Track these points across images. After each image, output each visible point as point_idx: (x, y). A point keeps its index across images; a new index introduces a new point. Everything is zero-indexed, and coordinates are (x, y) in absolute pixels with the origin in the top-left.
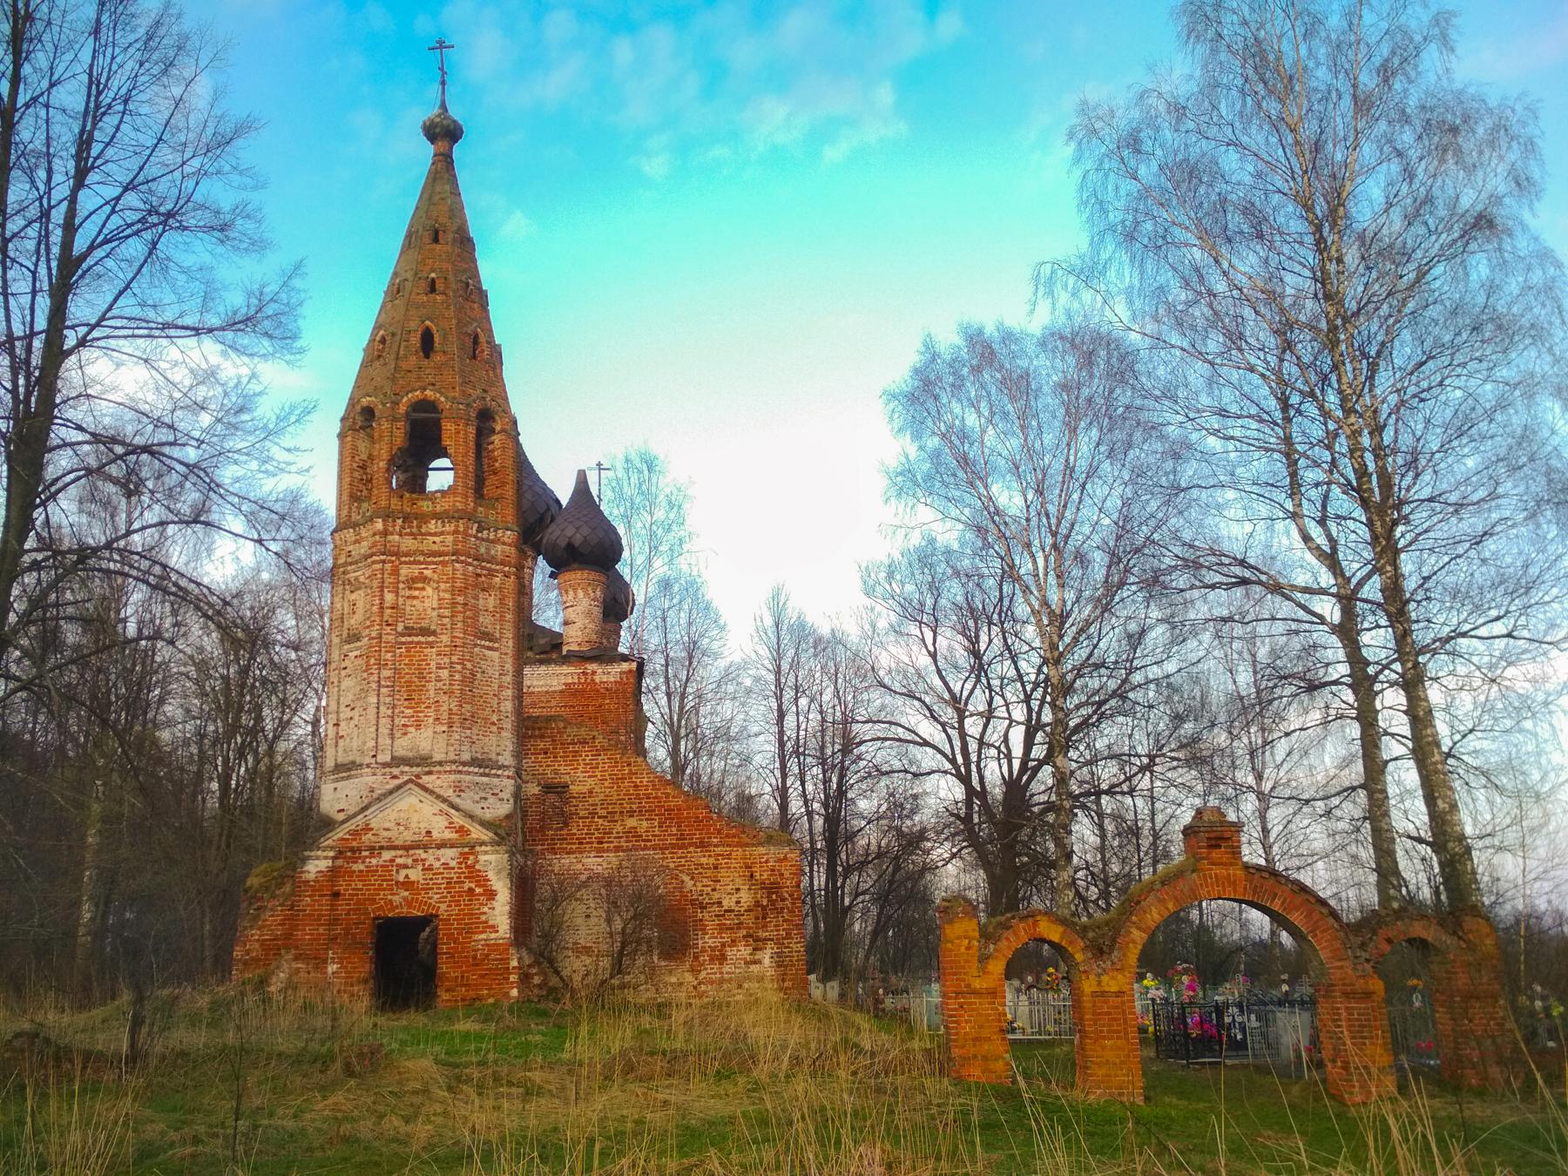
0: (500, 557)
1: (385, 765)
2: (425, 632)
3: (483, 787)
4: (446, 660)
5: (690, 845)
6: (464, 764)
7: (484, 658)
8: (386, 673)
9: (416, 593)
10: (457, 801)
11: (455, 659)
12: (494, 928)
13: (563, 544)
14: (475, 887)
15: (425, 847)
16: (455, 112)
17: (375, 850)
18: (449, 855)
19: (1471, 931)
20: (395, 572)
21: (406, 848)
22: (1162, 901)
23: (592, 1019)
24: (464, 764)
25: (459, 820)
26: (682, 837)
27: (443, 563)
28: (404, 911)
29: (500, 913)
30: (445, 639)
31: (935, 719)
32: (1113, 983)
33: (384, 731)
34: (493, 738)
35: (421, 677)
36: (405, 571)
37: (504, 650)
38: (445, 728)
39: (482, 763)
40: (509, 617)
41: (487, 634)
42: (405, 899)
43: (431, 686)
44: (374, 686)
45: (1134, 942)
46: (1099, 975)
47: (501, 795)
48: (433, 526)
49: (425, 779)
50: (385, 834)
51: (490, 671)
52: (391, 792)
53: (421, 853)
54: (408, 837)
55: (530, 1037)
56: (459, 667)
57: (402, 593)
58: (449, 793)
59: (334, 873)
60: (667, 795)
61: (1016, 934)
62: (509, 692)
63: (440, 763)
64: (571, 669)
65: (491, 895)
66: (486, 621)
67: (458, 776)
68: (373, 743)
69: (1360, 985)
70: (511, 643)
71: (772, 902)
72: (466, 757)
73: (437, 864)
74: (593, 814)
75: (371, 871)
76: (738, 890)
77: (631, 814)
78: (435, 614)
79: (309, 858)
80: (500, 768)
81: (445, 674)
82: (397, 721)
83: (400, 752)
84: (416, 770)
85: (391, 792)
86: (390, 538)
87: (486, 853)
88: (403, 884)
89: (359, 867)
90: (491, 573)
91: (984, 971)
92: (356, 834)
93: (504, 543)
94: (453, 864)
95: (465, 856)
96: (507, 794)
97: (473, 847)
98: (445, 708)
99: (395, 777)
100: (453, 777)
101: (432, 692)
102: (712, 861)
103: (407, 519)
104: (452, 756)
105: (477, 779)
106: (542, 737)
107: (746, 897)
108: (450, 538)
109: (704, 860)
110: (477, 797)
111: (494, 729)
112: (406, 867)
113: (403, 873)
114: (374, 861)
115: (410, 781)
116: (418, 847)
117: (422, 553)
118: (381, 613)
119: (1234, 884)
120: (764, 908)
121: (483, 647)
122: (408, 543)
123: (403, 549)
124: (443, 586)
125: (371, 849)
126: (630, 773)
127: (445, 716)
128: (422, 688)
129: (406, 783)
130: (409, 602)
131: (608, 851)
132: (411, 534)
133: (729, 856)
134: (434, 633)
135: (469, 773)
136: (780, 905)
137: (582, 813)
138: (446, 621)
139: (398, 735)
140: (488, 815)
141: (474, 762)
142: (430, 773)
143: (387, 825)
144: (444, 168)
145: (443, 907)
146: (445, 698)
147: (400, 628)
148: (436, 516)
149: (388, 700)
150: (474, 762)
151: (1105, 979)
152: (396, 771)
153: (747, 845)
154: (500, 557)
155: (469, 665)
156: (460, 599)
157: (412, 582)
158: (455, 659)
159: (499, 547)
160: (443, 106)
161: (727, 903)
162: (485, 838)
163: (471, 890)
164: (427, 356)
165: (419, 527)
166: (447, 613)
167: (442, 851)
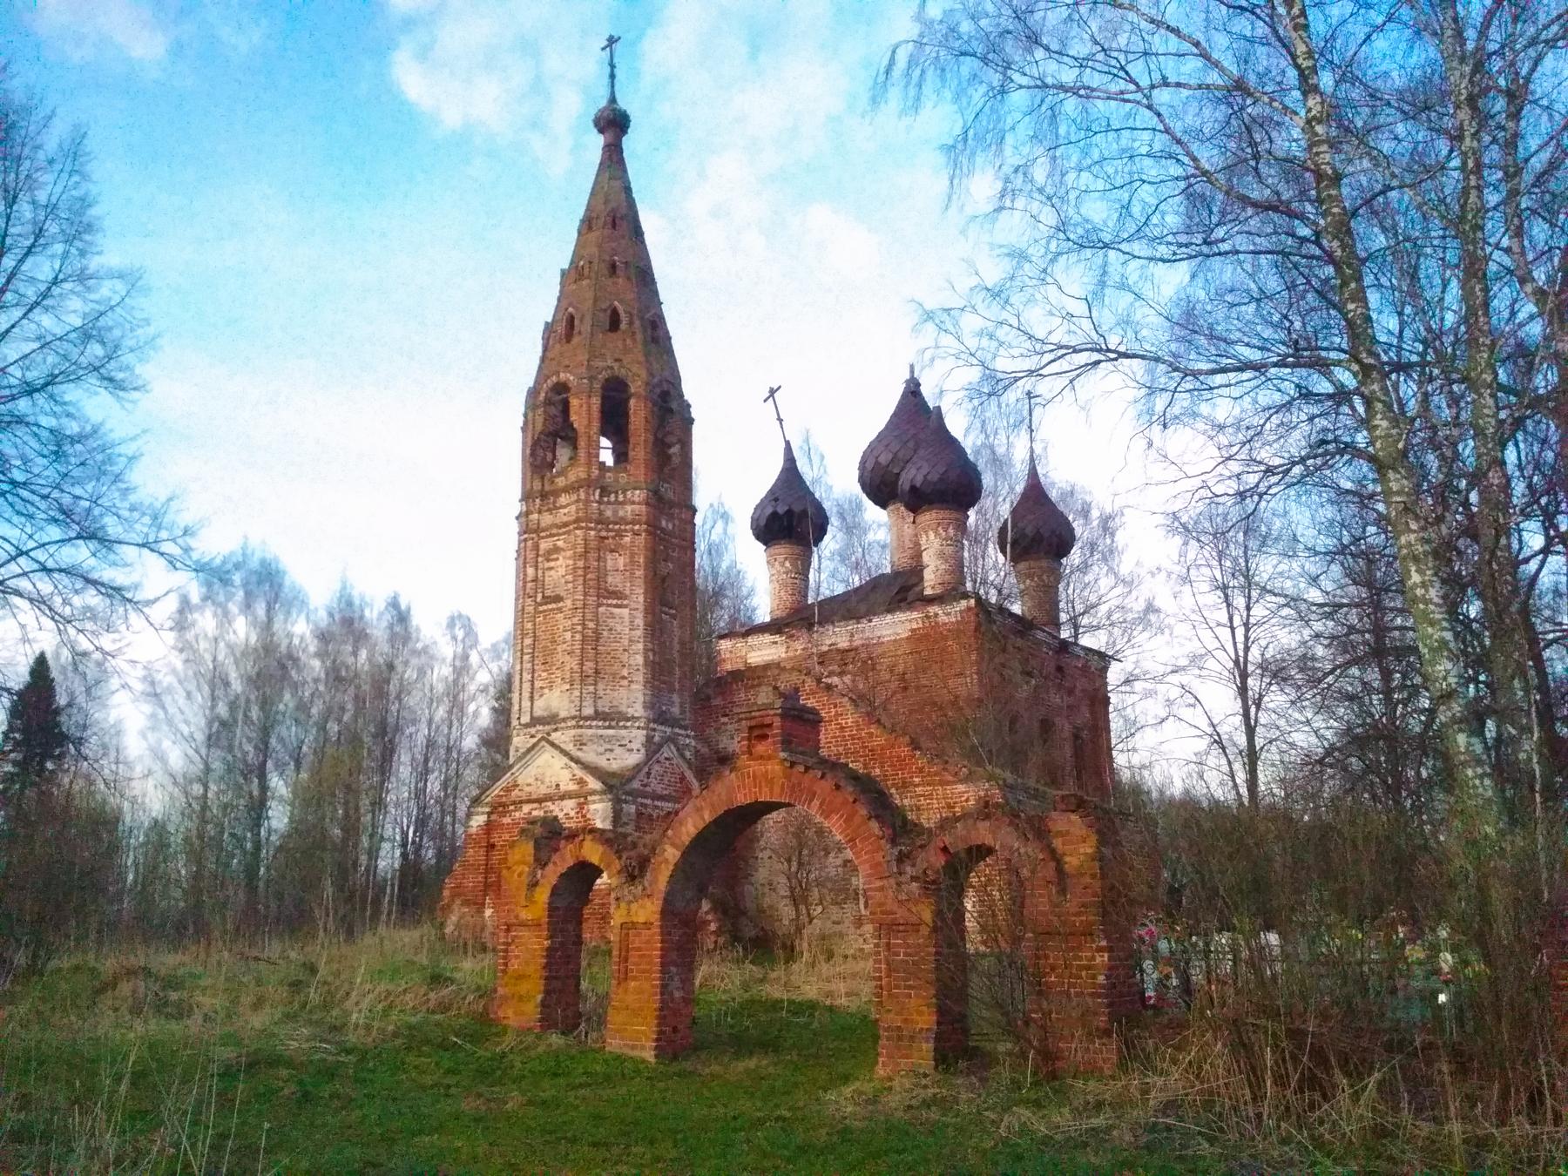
0: (630, 517)
1: (527, 726)
3: (609, 739)
6: (587, 718)
7: (613, 616)
16: (623, 104)
17: (519, 803)
18: (569, 804)
19: (1060, 834)
20: (536, 547)
21: (539, 801)
22: (699, 810)
23: (100, 943)
24: (587, 718)
25: (580, 773)
27: (568, 533)
30: (569, 603)
33: (526, 695)
37: (633, 605)
40: (640, 573)
41: (614, 593)
45: (666, 861)
46: (630, 902)
48: (563, 499)
49: (555, 736)
50: (527, 789)
51: (619, 628)
52: (529, 750)
54: (543, 790)
58: (570, 747)
59: (489, 827)
60: (871, 735)
62: (641, 646)
63: (564, 720)
64: (915, 615)
66: (614, 581)
67: (579, 731)
69: (901, 914)
70: (641, 599)
72: (589, 711)
80: (628, 720)
81: (568, 635)
83: (538, 713)
84: (547, 728)
89: (506, 820)
90: (620, 534)
91: (530, 899)
92: (508, 790)
93: (633, 503)
94: (572, 814)
95: (581, 806)
96: (636, 745)
100: (573, 732)
104: (574, 713)
105: (601, 732)
108: (573, 508)
110: (601, 749)
111: (625, 683)
115: (543, 738)
119: (770, 782)
122: (547, 519)
125: (514, 803)
126: (837, 715)
132: (549, 510)
133: (930, 796)
135: (590, 727)
141: (598, 715)
144: (613, 157)
148: (566, 490)
150: (598, 715)
151: (634, 906)
152: (533, 731)
153: (948, 783)
154: (630, 517)
158: (575, 620)
159: (629, 508)
160: (613, 100)
164: (568, 341)
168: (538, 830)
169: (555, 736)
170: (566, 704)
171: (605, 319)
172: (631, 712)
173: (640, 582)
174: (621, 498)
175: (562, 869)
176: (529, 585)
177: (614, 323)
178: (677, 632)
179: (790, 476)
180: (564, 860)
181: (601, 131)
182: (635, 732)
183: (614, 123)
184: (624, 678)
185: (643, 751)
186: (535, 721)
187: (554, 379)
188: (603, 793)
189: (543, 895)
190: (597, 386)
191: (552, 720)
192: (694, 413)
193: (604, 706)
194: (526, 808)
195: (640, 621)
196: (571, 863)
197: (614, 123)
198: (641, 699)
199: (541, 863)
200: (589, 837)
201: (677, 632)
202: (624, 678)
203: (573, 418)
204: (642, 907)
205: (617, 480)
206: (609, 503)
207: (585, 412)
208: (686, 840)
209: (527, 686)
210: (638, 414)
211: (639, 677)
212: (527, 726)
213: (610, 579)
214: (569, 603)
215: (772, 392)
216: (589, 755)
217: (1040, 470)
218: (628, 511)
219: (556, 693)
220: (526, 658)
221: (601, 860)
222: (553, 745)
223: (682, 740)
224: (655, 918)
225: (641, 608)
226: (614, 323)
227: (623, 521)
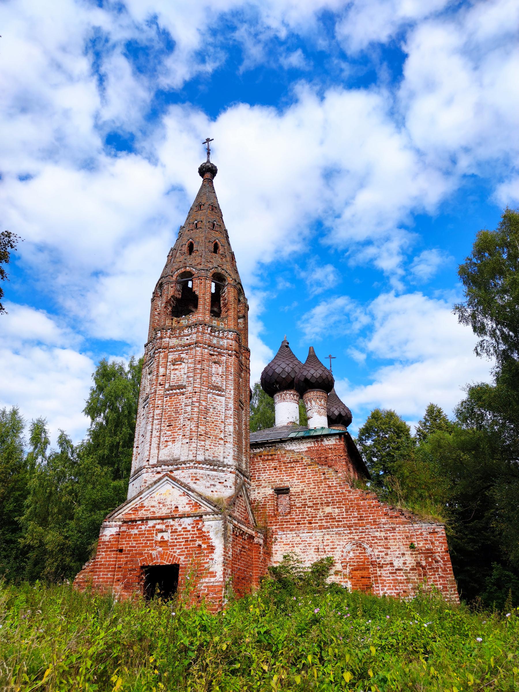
1: (154, 466)
4: (190, 401)
5: (367, 523)
6: (199, 463)
8: (157, 412)
9: (176, 367)
10: (192, 486)
11: (194, 399)
12: (213, 574)
13: (303, 379)
14: (202, 546)
15: (173, 518)
18: (187, 522)
20: (166, 357)
21: (162, 519)
24: (199, 463)
26: (361, 519)
28: (159, 562)
29: (217, 563)
30: (190, 389)
33: (154, 445)
34: (221, 448)
35: (177, 412)
36: (171, 357)
37: (228, 396)
38: (188, 441)
39: (214, 464)
40: (231, 377)
42: (159, 552)
43: (181, 417)
44: (150, 419)
47: (225, 484)
49: (176, 474)
51: (219, 408)
52: (155, 483)
53: (171, 522)
54: (164, 512)
55: (514, 630)
56: (197, 404)
57: (169, 367)
58: (188, 481)
62: (232, 420)
65: (212, 549)
66: (216, 380)
67: (195, 470)
68: (148, 453)
70: (232, 392)
71: (430, 564)
72: (200, 458)
73: (180, 529)
74: (305, 505)
75: (141, 534)
76: (403, 554)
77: (328, 504)
78: (186, 376)
79: (106, 527)
80: (224, 466)
81: (189, 409)
82: (162, 439)
83: (162, 458)
84: (171, 467)
85: (155, 483)
86: (164, 340)
87: (209, 520)
88: (160, 542)
92: (136, 510)
93: (228, 339)
94: (189, 528)
97: (201, 516)
98: (188, 428)
99: (159, 473)
101: (182, 420)
102: (383, 534)
103: (173, 329)
104: (191, 458)
106: (273, 460)
107: (410, 560)
109: (377, 534)
110: (208, 484)
111: (222, 442)
112: (162, 531)
113: (160, 535)
114: (143, 527)
115: (167, 475)
116: (169, 518)
117: (181, 346)
118: (157, 379)
120: (424, 568)
121: (213, 394)
122: (174, 342)
123: (171, 344)
124: (190, 361)
125: (142, 520)
126: (325, 479)
127: (188, 433)
128: (176, 419)
129: (164, 476)
130: (172, 372)
131: (315, 528)
134: (184, 387)
135: (202, 468)
136: (435, 565)
137: (298, 505)
138: (191, 379)
139: (162, 447)
140: (215, 496)
141: (206, 462)
142: (178, 469)
143: (153, 504)
145: (182, 558)
146: (189, 422)
147: (167, 386)
149: (158, 427)
152: (159, 469)
155: (204, 403)
156: (199, 366)
159: (225, 341)
160: (208, 161)
162: (209, 510)
163: (200, 546)
165: (180, 333)
166: (191, 374)
167: (182, 520)
169: (176, 474)
170: (185, 451)
172: (226, 461)
174: (221, 335)
176: (161, 378)
182: (229, 475)
183: (208, 172)
184: (221, 439)
185: (233, 487)
187: (183, 270)
188: (215, 513)
193: (209, 455)
194: (151, 523)
195: (231, 405)
197: (208, 172)
198: (232, 454)
202: (221, 439)
205: (218, 325)
206: (214, 336)
209: (155, 440)
210: (229, 294)
213: (214, 379)
214: (190, 389)
216: (201, 487)
217: (385, 370)
218: (225, 343)
219: (178, 444)
220: (156, 422)
222: (174, 479)
225: (232, 397)
227: (221, 347)
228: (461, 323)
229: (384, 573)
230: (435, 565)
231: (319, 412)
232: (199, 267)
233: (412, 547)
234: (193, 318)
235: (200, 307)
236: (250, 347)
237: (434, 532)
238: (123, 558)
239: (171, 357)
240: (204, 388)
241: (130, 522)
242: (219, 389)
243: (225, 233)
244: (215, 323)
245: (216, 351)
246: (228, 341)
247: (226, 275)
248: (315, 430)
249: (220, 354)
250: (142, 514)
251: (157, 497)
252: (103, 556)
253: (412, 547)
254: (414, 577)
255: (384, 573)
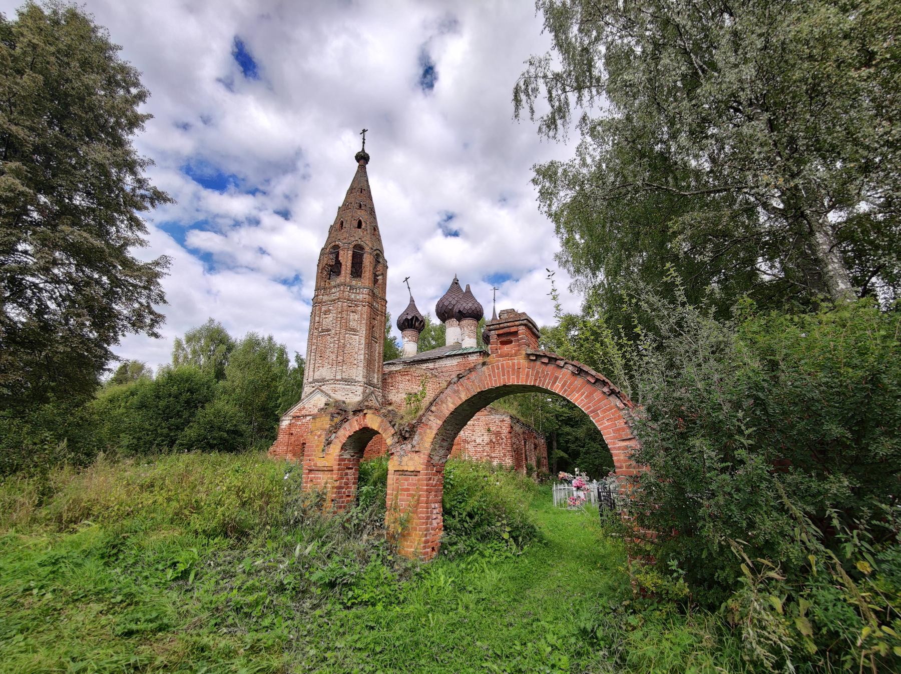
1: (311, 383)
2: (328, 330)
8: (314, 347)
16: (366, 151)
20: (320, 309)
31: (247, 267)
32: (411, 463)
33: (311, 369)
36: (323, 309)
39: (348, 381)
46: (401, 456)
61: (351, 426)
66: (353, 324)
71: (498, 440)
72: (339, 377)
83: (316, 377)
92: (300, 410)
107: (486, 439)
122: (325, 298)
136: (501, 441)
141: (342, 379)
144: (362, 172)
151: (405, 459)
157: (325, 313)
160: (363, 150)
161: (479, 441)
168: (331, 410)
171: (356, 224)
172: (357, 379)
173: (364, 326)
175: (348, 434)
177: (359, 225)
178: (377, 348)
179: (412, 305)
180: (353, 426)
181: (358, 161)
183: (362, 158)
186: (315, 381)
189: (335, 450)
190: (351, 246)
191: (323, 381)
192: (388, 264)
195: (363, 341)
196: (357, 428)
197: (362, 158)
199: (336, 428)
200: (369, 411)
201: (377, 348)
203: (340, 258)
204: (411, 459)
207: (346, 258)
208: (447, 413)
209: (312, 366)
210: (367, 260)
211: (361, 365)
212: (311, 383)
214: (333, 331)
215: (364, 131)
218: (360, 297)
219: (325, 369)
221: (379, 427)
222: (322, 391)
223: (377, 393)
224: (421, 467)
226: (359, 225)
227: (358, 300)
228: (266, 337)
229: (470, 447)
230: (501, 441)
231: (469, 337)
232: (345, 241)
233: (489, 430)
234: (340, 279)
235: (343, 272)
236: (387, 299)
237: (503, 421)
238: (293, 439)
239: (323, 309)
240: (343, 331)
241: (296, 417)
242: (354, 330)
243: (372, 212)
244: (354, 283)
245: (353, 305)
246: (363, 295)
247: (365, 245)
248: (466, 349)
249: (356, 305)
250: (304, 412)
251: (312, 402)
252: (282, 438)
253: (489, 430)
254: (487, 448)
255: (470, 447)
